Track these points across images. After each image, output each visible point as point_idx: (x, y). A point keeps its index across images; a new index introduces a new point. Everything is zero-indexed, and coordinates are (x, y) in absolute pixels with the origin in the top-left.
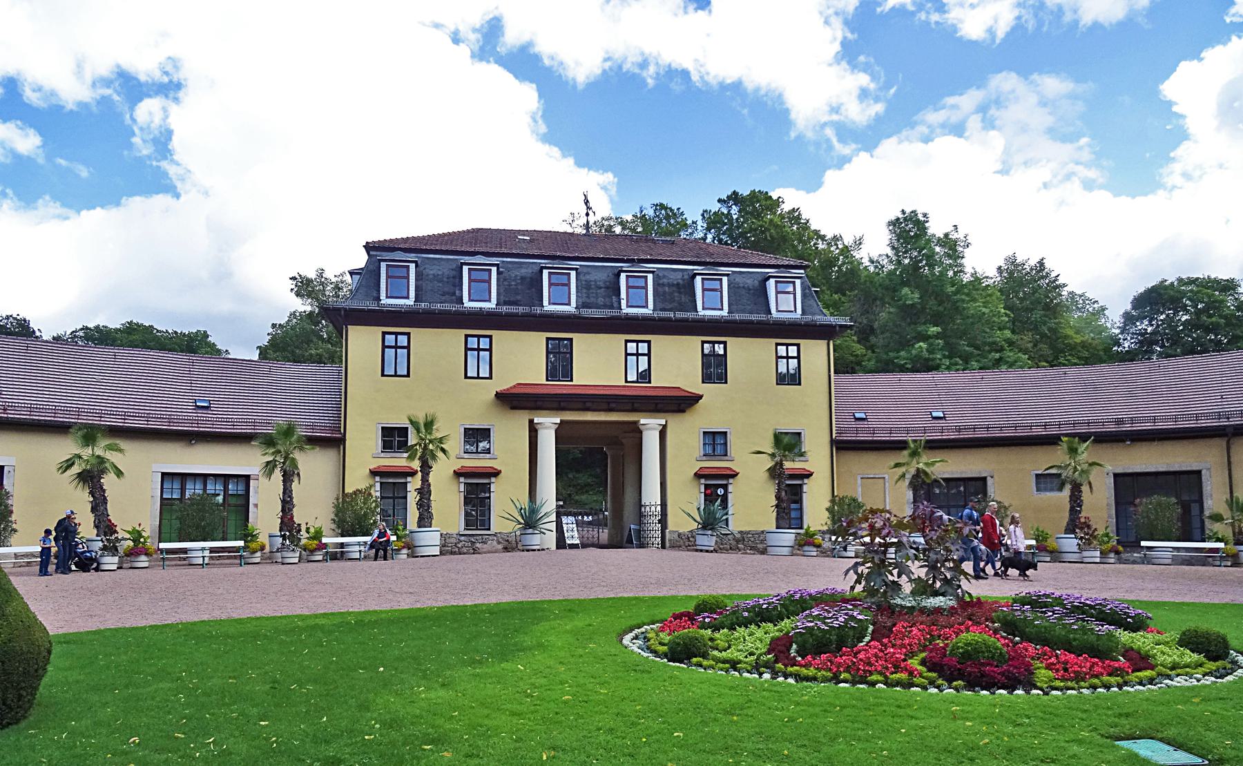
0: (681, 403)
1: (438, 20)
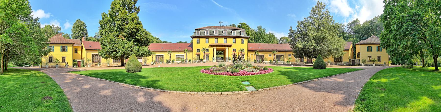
0: (230, 46)
1: (381, 58)
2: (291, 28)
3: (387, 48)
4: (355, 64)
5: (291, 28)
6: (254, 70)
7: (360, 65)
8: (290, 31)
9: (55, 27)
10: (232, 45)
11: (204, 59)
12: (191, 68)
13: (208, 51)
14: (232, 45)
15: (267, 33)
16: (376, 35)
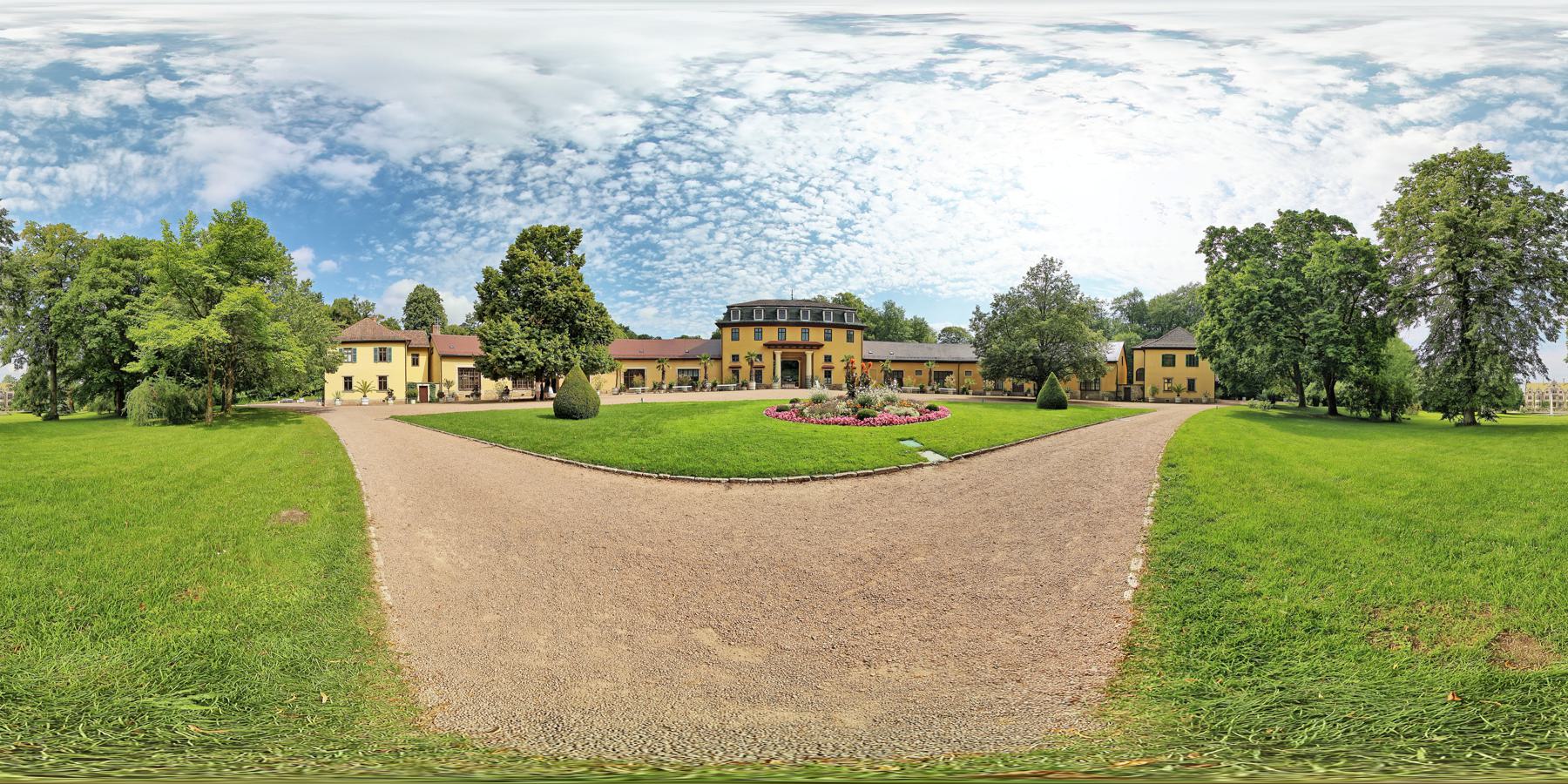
0: (819, 346)
2: (978, 309)
3: (1211, 360)
4: (1132, 398)
5: (978, 309)
6: (910, 410)
7: (1143, 399)
8: (974, 316)
9: (360, 301)
10: (822, 345)
11: (751, 380)
12: (744, 403)
13: (761, 360)
14: (822, 345)
15: (908, 316)
16: (1184, 327)
